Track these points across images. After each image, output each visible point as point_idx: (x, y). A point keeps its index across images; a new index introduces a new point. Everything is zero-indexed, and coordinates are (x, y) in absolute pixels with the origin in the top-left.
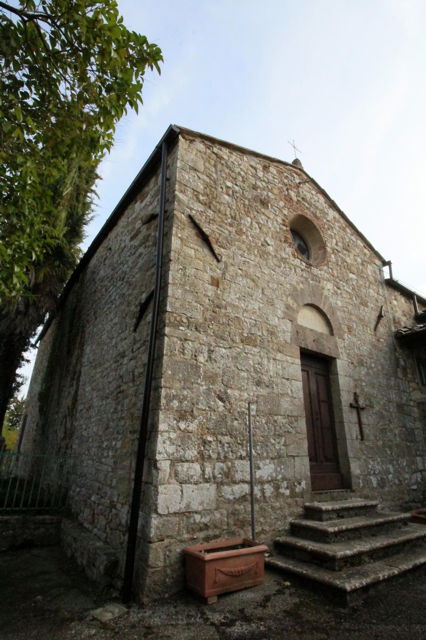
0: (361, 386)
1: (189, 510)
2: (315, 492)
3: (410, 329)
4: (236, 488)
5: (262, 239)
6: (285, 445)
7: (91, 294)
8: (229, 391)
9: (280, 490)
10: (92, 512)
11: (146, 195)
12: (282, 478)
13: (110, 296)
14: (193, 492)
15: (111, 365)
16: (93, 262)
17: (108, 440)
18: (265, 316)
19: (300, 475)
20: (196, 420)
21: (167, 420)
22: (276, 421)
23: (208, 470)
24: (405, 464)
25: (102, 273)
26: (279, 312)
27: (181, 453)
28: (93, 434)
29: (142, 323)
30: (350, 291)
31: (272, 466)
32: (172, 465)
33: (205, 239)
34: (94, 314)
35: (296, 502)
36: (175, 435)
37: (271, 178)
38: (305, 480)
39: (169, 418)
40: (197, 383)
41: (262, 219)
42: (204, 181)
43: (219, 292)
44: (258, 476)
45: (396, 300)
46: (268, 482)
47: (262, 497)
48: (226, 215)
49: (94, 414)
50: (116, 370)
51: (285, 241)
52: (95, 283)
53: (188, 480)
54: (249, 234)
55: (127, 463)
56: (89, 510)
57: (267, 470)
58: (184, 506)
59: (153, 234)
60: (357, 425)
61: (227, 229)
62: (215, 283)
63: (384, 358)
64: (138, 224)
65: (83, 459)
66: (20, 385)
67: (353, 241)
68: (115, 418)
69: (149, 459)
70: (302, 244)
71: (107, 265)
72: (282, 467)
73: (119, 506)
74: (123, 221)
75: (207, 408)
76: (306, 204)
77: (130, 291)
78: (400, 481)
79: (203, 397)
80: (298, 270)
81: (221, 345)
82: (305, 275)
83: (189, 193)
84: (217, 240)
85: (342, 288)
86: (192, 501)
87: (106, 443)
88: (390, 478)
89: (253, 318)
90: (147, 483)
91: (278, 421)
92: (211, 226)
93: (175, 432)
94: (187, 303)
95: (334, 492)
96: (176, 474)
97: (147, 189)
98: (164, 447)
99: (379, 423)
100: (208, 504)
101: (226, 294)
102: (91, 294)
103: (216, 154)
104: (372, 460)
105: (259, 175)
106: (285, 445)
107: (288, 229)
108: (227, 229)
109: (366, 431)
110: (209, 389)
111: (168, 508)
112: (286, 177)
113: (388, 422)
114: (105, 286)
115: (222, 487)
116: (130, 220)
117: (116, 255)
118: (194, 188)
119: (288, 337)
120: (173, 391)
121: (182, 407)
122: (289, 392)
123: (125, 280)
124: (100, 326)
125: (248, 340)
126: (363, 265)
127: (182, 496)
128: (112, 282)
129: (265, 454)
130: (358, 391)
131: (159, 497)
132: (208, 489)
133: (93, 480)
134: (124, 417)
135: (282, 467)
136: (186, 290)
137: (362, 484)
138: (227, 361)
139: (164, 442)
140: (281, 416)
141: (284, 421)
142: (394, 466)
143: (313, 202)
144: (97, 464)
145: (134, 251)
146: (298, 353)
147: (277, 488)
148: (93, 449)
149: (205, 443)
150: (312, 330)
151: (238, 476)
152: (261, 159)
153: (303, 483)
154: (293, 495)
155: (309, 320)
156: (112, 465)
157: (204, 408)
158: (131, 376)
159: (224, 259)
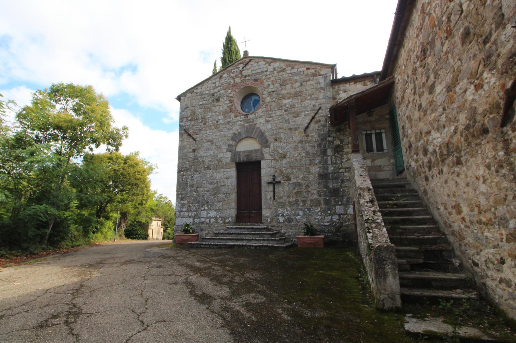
6: (222, 205)
57: (212, 214)
106: (222, 205)
125: (208, 168)
146: (234, 165)
149: (190, 206)
159: (198, 139)
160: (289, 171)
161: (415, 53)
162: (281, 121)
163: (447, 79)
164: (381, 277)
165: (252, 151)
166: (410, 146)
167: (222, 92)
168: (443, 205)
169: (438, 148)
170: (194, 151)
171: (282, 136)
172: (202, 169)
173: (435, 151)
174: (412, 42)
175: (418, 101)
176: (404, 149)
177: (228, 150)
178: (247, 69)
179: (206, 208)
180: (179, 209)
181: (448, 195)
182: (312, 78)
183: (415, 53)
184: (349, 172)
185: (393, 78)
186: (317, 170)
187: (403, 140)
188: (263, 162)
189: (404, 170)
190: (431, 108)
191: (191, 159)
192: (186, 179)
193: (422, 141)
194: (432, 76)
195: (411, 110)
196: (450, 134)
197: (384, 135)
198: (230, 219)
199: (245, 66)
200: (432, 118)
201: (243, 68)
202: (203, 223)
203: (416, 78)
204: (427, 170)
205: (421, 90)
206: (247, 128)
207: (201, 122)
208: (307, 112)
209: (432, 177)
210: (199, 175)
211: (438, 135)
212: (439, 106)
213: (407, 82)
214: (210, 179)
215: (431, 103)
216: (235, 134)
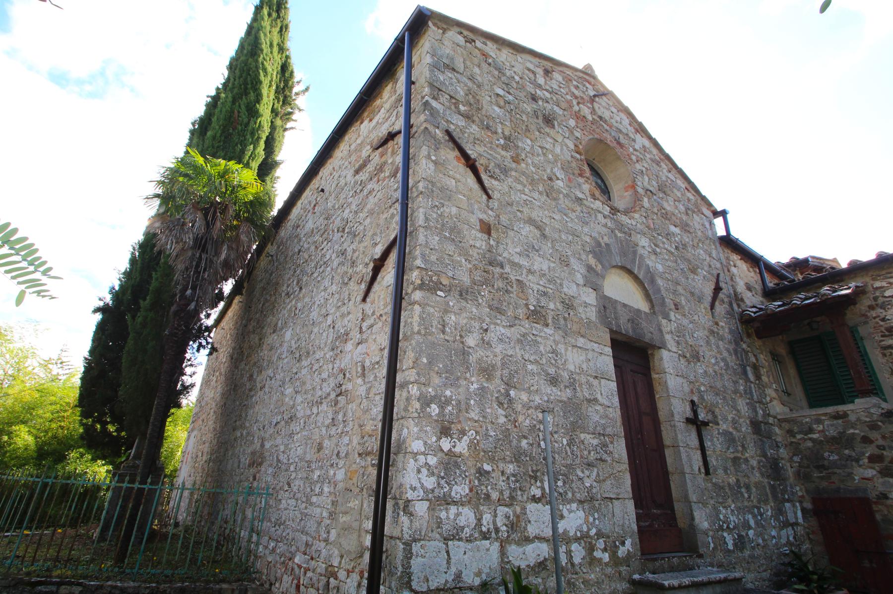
0: (699, 391)
1: (461, 585)
2: (648, 557)
3: (761, 309)
4: (529, 548)
5: (549, 171)
7: (293, 255)
9: (595, 554)
10: (295, 582)
11: (377, 110)
12: (596, 534)
13: (324, 256)
14: (465, 553)
15: (325, 354)
16: (296, 211)
17: (321, 468)
18: (558, 281)
19: (622, 530)
20: (465, 437)
21: (423, 435)
22: (583, 442)
23: (487, 518)
24: (769, 513)
25: (310, 225)
26: (579, 276)
27: (445, 490)
28: (297, 460)
29: (376, 287)
30: (673, 250)
31: (581, 514)
32: (431, 509)
34: (298, 283)
35: (620, 573)
36: (435, 459)
37: (555, 87)
38: (630, 537)
39: (426, 431)
40: (466, 379)
41: (548, 143)
42: (466, 86)
43: (492, 242)
44: (561, 531)
45: (735, 266)
46: (577, 540)
47: (569, 564)
48: (496, 133)
49: (298, 428)
50: (333, 362)
51: (581, 175)
52: (300, 240)
53: (457, 534)
54: (530, 161)
55: (354, 504)
56: (291, 578)
57: (573, 520)
58: (453, 577)
59: (390, 161)
60: (699, 452)
61: (499, 154)
62: (487, 229)
63: (728, 350)
64: (366, 151)
65: (280, 497)
66: (186, 389)
67: (672, 180)
68: (332, 433)
69: (395, 498)
70: (599, 181)
71: (318, 214)
72: (596, 515)
73: (342, 574)
74: (343, 149)
75: (481, 419)
76: (605, 126)
77: (354, 246)
78: (764, 540)
79: (475, 400)
80: (600, 216)
81: (499, 321)
82: (609, 224)
83: (444, 98)
84: (486, 170)
85: (661, 245)
86: (463, 570)
87: (317, 473)
88: (751, 536)
89: (541, 283)
90: (391, 538)
91: (586, 442)
92: (478, 148)
93: (435, 455)
94: (446, 257)
95: (673, 557)
97: (378, 102)
98: (419, 479)
99: (728, 449)
100: (488, 574)
101: (501, 246)
102: (293, 255)
103: (479, 50)
104: (724, 507)
105: (539, 82)
107: (583, 157)
108: (499, 154)
109: (713, 461)
110: (482, 388)
111: (428, 581)
112: (577, 87)
113: (740, 448)
114: (315, 242)
115: (507, 546)
116: (353, 147)
117: (331, 199)
118: (452, 94)
119: (592, 314)
120: (430, 390)
121: (444, 416)
123: (346, 230)
124: (306, 300)
125: (537, 315)
126: (687, 214)
127: (448, 562)
128: (324, 236)
129: (570, 495)
130: (695, 399)
131: (412, 562)
132: (488, 550)
133: (298, 531)
134: (347, 432)
135: (596, 515)
136: (445, 237)
137: (712, 545)
138: (507, 346)
139: (419, 471)
140: (589, 433)
141: (595, 442)
142: (754, 516)
143: (615, 124)
144: (304, 505)
145: (360, 188)
146: (607, 337)
147: (591, 549)
148: (297, 483)
149: (481, 473)
150: (625, 305)
151: (532, 530)
153: (628, 542)
154: (616, 561)
155: (621, 289)
156: (329, 507)
157: (476, 419)
158: (359, 369)
159: (496, 195)
164: (166, 263)
180: (430, 482)
184: (603, 101)
192: (463, 332)
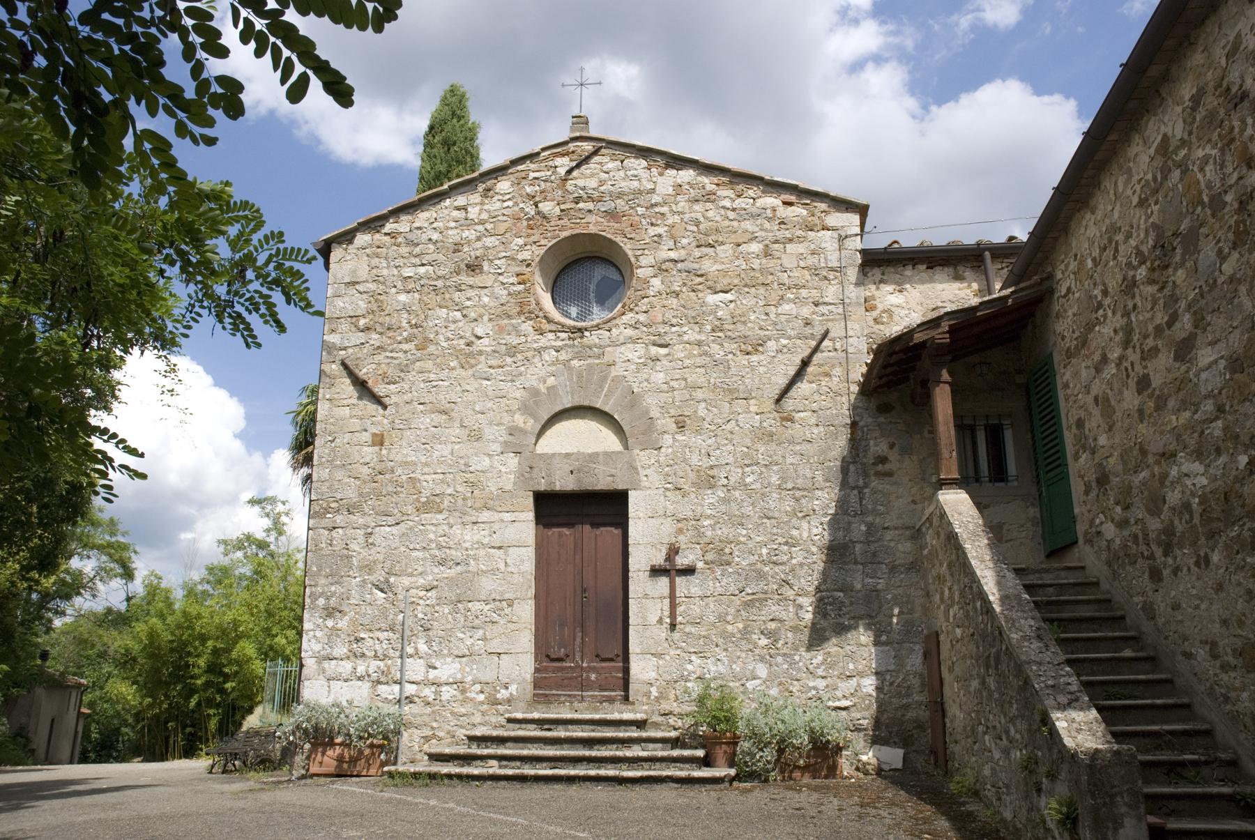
8: (392, 580)
33: (361, 385)
57: (447, 669)
61: (401, 350)
62: (379, 441)
83: (344, 326)
96: (324, 671)
122: (502, 566)
125: (430, 506)
129: (445, 652)
146: (530, 502)
152: (461, 200)
160: (724, 531)
161: (1133, 242)
162: (699, 361)
163: (1231, 340)
165: (597, 454)
166: (1103, 480)
167: (489, 241)
168: (1207, 648)
169: (1197, 500)
170: (379, 441)
171: (702, 410)
172: (410, 509)
173: (1187, 506)
174: (1118, 203)
175: (1138, 367)
176: (1077, 487)
177: (507, 447)
178: (584, 176)
179: (423, 647)
181: (1225, 622)
182: (799, 233)
183: (1133, 242)
185: (1050, 277)
186: (815, 531)
187: (1076, 457)
188: (632, 496)
189: (1076, 542)
190: (1181, 395)
191: (365, 470)
193: (1144, 474)
194: (1186, 320)
195: (1109, 383)
196: (1234, 473)
197: (1008, 435)
198: (513, 688)
199: (578, 166)
200: (1182, 421)
201: (570, 172)
202: (410, 699)
203: (1135, 307)
204: (1158, 552)
205: (1150, 342)
206: (580, 376)
207: (407, 340)
208: (785, 342)
209: (1176, 571)
210: (395, 530)
211: (1197, 467)
212: (1206, 397)
213: (1100, 305)
214: (440, 547)
215: (1182, 383)
216: (535, 393)
